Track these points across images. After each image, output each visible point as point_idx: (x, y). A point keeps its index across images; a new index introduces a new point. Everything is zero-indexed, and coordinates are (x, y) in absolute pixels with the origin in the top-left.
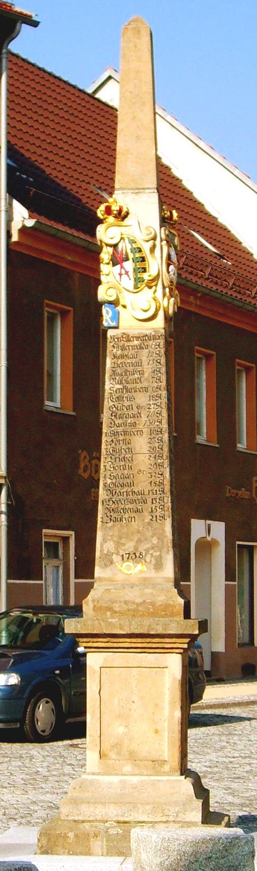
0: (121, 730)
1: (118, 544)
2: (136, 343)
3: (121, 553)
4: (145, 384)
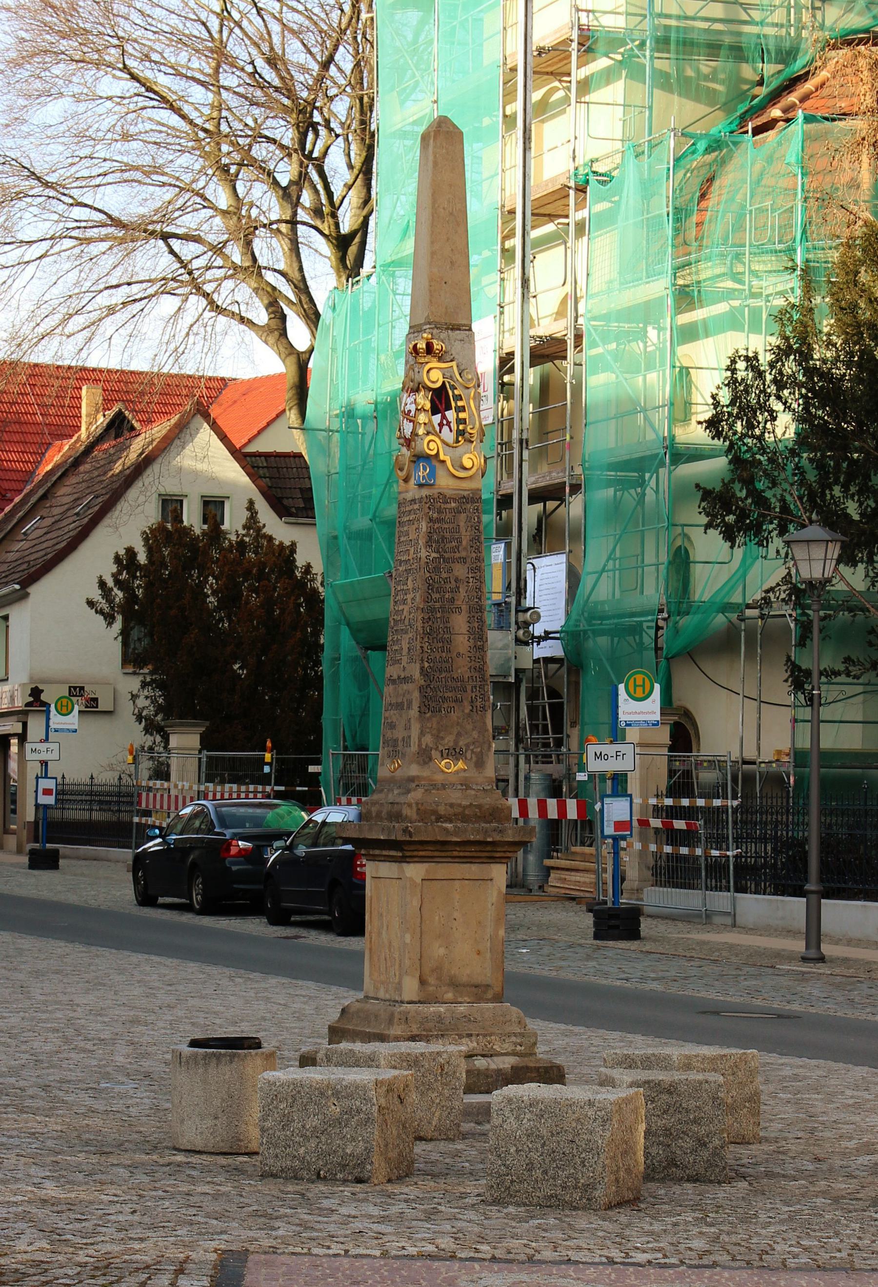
0: (442, 951)
1: (438, 738)
2: (453, 505)
3: (441, 748)
4: (463, 554)
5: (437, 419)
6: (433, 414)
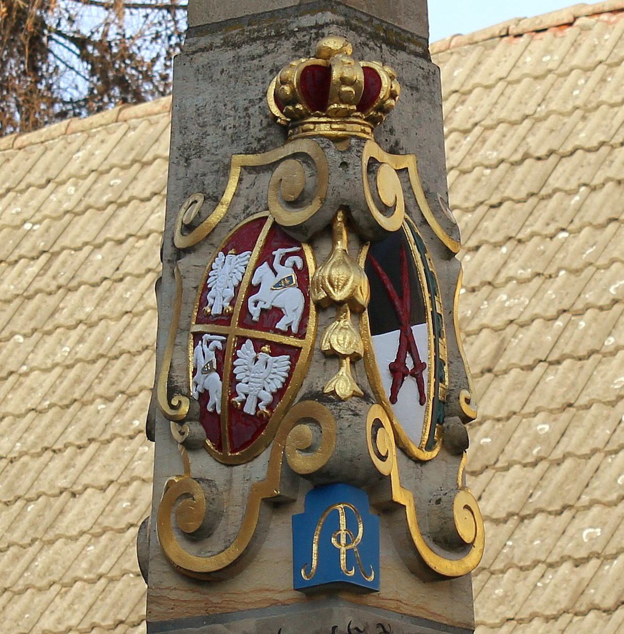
5: (386, 346)
6: (377, 328)
